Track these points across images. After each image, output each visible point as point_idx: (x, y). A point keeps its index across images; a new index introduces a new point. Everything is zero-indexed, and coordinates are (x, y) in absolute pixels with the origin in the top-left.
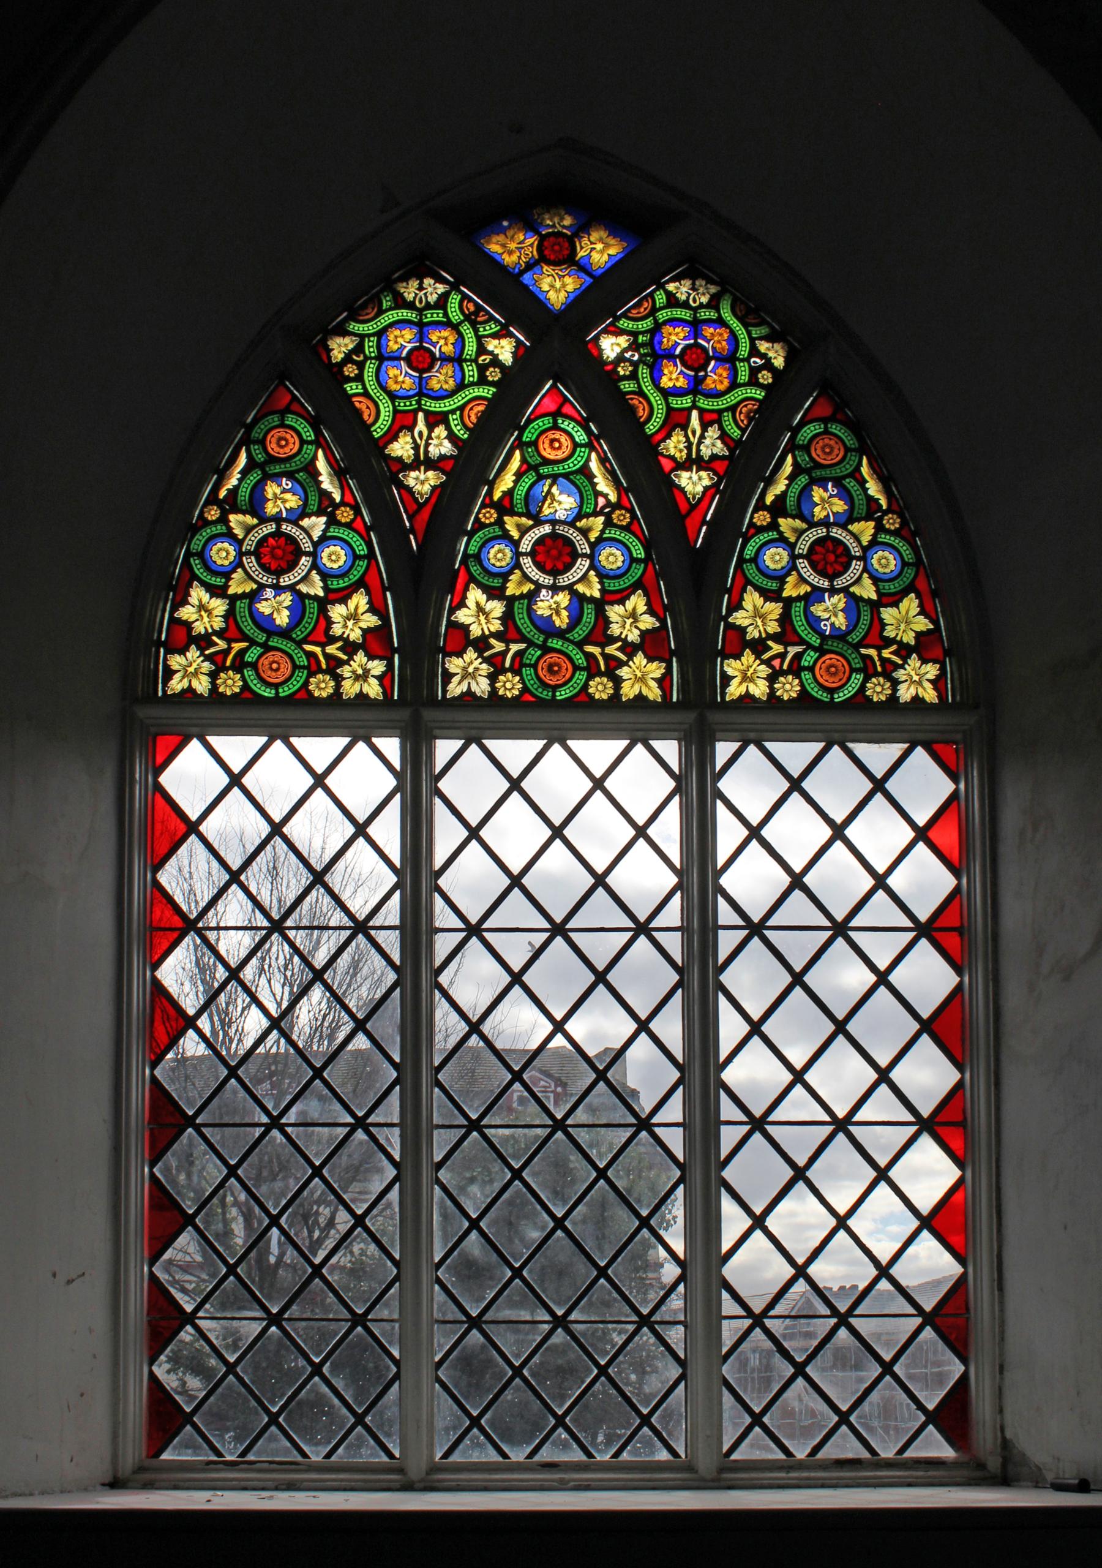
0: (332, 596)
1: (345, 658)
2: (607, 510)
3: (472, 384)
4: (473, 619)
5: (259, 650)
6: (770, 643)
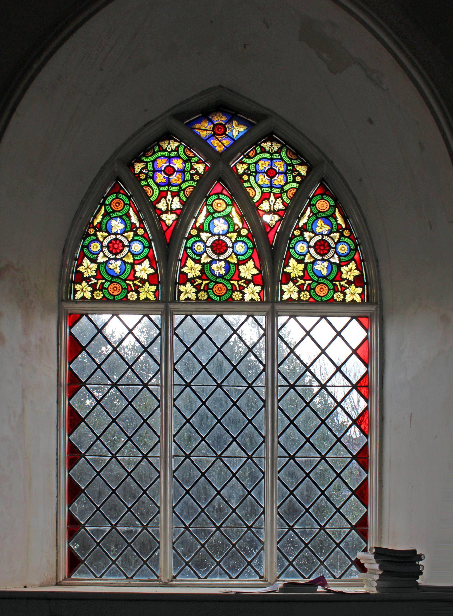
0: (136, 262)
1: (348, 286)
2: (134, 229)
3: (188, 181)
4: (139, 271)
5: (316, 284)
6: (92, 278)
